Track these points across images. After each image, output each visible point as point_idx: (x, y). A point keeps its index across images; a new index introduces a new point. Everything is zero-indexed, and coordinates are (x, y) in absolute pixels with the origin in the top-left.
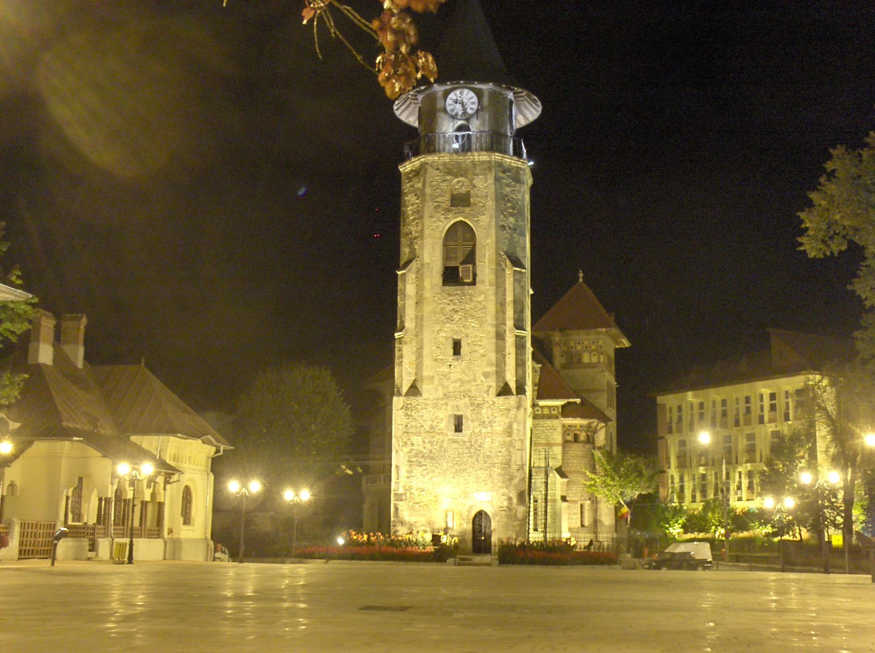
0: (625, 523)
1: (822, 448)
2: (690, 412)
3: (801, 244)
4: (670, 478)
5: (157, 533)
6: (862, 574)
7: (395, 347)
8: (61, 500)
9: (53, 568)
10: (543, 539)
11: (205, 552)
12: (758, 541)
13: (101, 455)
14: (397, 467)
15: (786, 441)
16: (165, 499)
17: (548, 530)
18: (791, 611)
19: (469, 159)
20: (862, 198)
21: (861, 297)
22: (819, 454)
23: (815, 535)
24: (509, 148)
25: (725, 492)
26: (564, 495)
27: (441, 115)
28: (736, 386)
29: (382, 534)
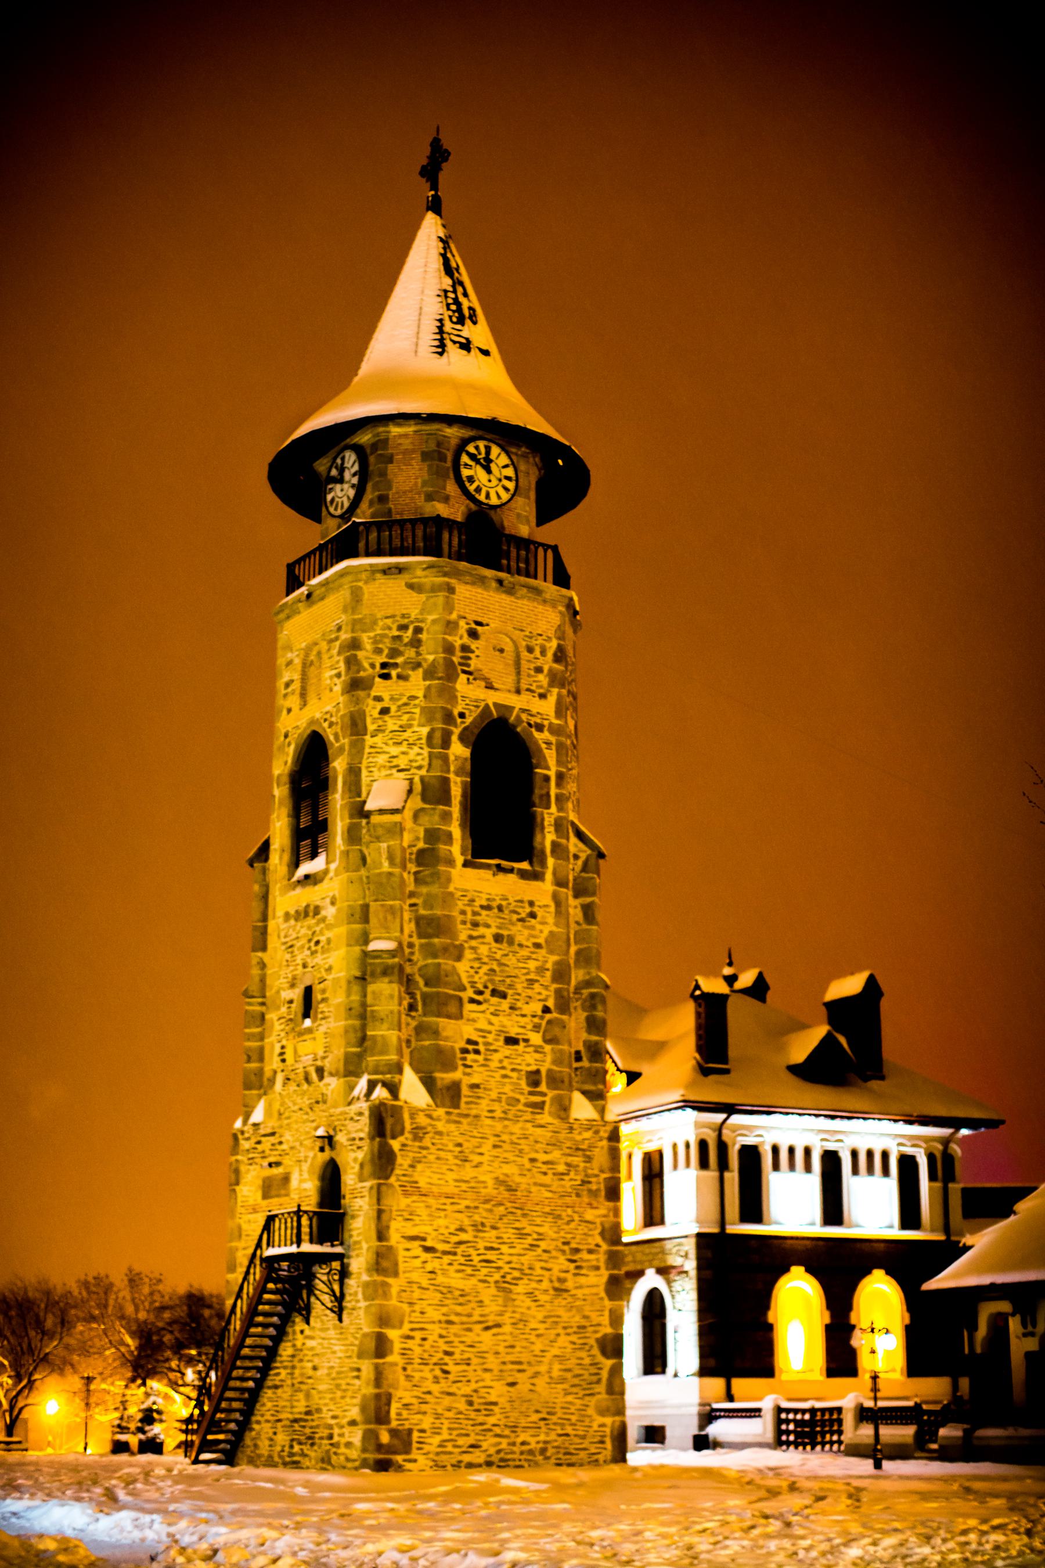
1: (356, 1338)
10: (871, 1440)
12: (560, 612)
14: (400, 569)
21: (605, 1336)
22: (691, 1265)
25: (635, 1538)
26: (669, 1433)
27: (492, 513)
28: (305, 519)
29: (803, 1420)
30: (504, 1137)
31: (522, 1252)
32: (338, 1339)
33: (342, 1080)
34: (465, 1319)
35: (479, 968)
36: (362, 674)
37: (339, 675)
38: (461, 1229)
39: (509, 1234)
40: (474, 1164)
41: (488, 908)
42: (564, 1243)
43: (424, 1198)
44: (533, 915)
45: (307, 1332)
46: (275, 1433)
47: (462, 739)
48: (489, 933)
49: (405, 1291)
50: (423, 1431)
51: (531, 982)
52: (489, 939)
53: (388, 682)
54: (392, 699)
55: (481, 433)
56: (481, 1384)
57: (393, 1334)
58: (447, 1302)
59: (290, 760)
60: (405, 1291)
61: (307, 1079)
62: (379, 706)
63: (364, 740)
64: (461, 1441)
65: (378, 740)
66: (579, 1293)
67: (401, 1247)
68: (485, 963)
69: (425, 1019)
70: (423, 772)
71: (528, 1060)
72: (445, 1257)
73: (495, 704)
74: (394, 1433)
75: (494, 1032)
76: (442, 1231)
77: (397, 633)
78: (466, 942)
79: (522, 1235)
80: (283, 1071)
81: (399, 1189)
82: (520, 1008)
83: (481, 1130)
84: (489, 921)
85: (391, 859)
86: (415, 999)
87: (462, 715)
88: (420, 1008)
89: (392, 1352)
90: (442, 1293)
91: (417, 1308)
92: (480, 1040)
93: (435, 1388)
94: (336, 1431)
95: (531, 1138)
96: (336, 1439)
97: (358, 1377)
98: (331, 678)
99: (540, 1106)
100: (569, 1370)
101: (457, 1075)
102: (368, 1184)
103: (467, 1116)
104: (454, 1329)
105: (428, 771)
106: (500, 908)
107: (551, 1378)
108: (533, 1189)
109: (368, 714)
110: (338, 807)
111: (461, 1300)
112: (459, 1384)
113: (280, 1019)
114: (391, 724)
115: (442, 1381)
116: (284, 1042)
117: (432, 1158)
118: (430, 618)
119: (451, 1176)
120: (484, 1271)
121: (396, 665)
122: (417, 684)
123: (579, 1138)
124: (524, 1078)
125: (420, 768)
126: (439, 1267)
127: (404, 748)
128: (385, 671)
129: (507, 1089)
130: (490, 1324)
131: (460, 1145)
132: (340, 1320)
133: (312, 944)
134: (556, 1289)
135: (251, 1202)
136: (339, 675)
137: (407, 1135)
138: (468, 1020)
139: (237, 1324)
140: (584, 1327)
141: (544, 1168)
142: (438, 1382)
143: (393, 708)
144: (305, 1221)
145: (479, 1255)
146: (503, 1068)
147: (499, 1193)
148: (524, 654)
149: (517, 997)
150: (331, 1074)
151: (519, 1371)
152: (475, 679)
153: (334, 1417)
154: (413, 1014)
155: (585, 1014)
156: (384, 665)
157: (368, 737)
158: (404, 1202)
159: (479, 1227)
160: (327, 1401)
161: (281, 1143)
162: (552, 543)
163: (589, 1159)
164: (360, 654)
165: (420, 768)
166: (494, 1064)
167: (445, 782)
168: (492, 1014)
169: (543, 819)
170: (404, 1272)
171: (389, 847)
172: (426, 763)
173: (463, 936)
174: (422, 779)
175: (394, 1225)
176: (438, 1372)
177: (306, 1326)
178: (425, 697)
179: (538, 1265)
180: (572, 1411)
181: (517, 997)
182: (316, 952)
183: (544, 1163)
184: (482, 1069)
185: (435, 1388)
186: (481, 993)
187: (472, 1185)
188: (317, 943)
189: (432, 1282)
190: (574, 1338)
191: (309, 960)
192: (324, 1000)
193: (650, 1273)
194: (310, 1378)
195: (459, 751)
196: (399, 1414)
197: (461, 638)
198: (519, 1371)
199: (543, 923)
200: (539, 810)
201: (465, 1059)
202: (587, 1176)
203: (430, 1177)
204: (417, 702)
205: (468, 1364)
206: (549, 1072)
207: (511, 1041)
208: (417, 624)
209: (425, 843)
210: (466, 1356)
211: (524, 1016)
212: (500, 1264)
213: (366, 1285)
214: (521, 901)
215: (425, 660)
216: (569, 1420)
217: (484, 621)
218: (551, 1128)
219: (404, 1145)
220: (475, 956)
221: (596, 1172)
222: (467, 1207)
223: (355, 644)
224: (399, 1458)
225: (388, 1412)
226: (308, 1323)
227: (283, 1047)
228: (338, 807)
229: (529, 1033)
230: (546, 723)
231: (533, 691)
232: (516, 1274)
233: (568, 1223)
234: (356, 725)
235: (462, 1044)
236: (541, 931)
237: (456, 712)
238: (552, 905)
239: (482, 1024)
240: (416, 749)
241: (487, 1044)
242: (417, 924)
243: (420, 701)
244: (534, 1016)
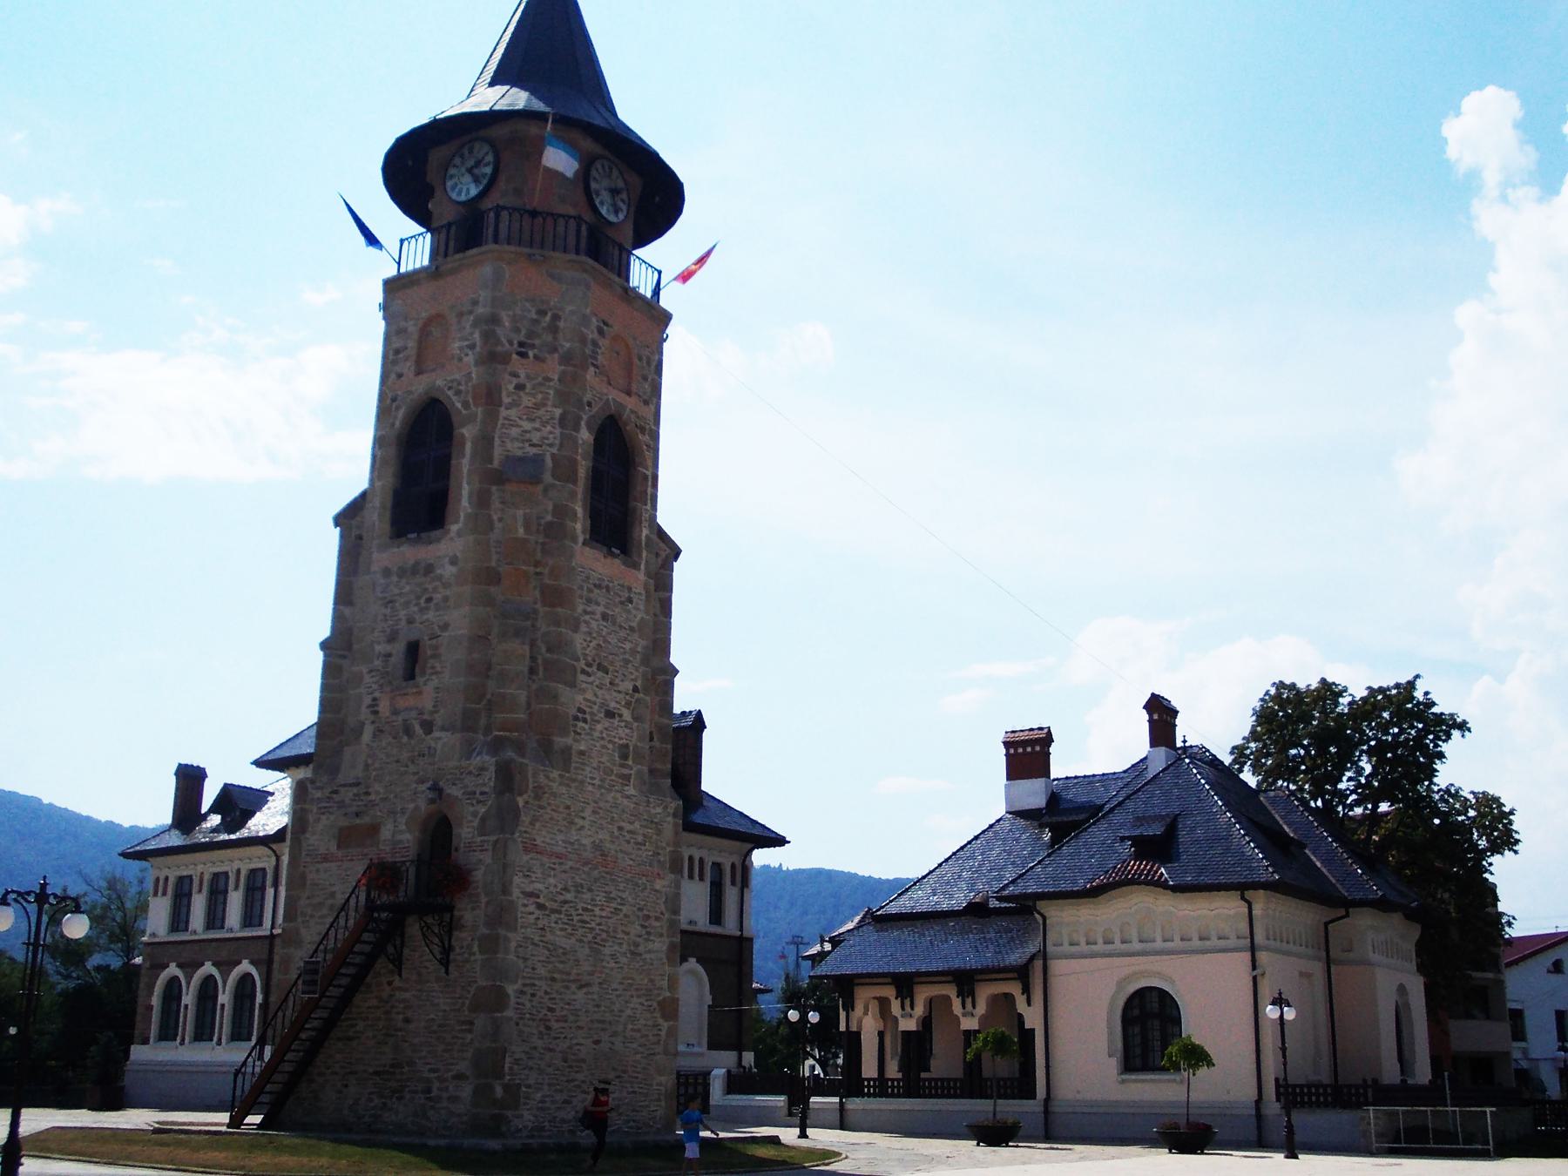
2: (1036, 732)
3: (1436, 764)
4: (219, 1007)
5: (550, 220)
6: (902, 1044)
7: (221, 1152)
8: (260, 1005)
9: (803, 1143)
11: (867, 987)
30: (602, 804)
31: (610, 915)
32: (442, 992)
33: (458, 735)
34: (564, 977)
35: (590, 642)
36: (499, 349)
37: (472, 347)
38: (566, 889)
39: (600, 898)
40: (578, 826)
41: (598, 586)
42: (639, 909)
43: (539, 856)
44: (630, 601)
46: (346, 1086)
47: (589, 428)
48: (600, 609)
49: (521, 946)
50: (529, 1086)
51: (627, 662)
52: (598, 616)
53: (524, 361)
54: (528, 377)
55: (607, 153)
56: (574, 1041)
58: (553, 959)
59: (398, 424)
60: (521, 946)
61: (408, 731)
62: (515, 381)
63: (498, 411)
64: (558, 1097)
65: (513, 413)
66: (648, 956)
67: (520, 902)
68: (594, 638)
69: (545, 683)
70: (554, 450)
71: (622, 734)
72: (553, 916)
73: (613, 399)
74: (506, 1088)
75: (598, 704)
76: (552, 889)
77: (535, 317)
78: (581, 615)
79: (610, 899)
80: (373, 722)
81: (521, 845)
82: (618, 685)
83: (584, 796)
84: (600, 600)
85: (527, 527)
87: (589, 404)
88: (541, 673)
90: (549, 950)
91: (529, 963)
92: (587, 710)
93: (539, 1043)
94: (436, 1085)
95: (620, 807)
96: (435, 1093)
97: (470, 1031)
98: (461, 348)
99: (627, 778)
100: (639, 1031)
101: (569, 741)
103: (574, 780)
104: (557, 986)
105: (558, 450)
106: (608, 588)
107: (625, 1037)
108: (620, 855)
109: (503, 387)
110: (465, 471)
111: (563, 959)
112: (558, 1041)
113: (371, 671)
114: (527, 401)
115: (545, 1037)
116: (377, 694)
117: (547, 817)
118: (570, 308)
119: (560, 837)
120: (581, 931)
121: (533, 346)
122: (554, 368)
123: (653, 811)
124: (617, 750)
125: (551, 445)
126: (547, 924)
127: (537, 425)
128: (523, 350)
129: (604, 759)
130: (583, 983)
131: (568, 807)
132: (447, 972)
133: (422, 601)
134: (633, 953)
135: (322, 850)
136: (472, 347)
137: (530, 793)
138: (580, 690)
140: (650, 990)
141: (628, 836)
142: (542, 1039)
143: (528, 386)
145: (578, 915)
146: (603, 738)
147: (595, 857)
148: (636, 360)
149: (616, 674)
150: (443, 729)
151: (603, 1030)
152: (600, 373)
153: (431, 1070)
154: (534, 677)
155: (658, 698)
156: (521, 344)
157: (502, 409)
159: (578, 888)
160: (424, 1054)
161: (368, 793)
162: (659, 269)
163: (659, 832)
164: (499, 331)
165: (551, 445)
166: (596, 734)
167: (573, 464)
168: (597, 686)
169: (641, 516)
170: (522, 927)
171: (525, 515)
172: (557, 442)
173: (580, 609)
174: (553, 455)
175: (517, 880)
176: (542, 1029)
177: (397, 978)
178: (559, 380)
179: (620, 928)
180: (638, 1070)
181: (616, 674)
182: (427, 609)
183: (628, 832)
184: (587, 737)
185: (539, 1043)
186: (589, 665)
187: (576, 847)
188: (429, 600)
189: (542, 939)
190: (642, 1000)
191: (417, 617)
192: (434, 656)
193: (173, 965)
194: (400, 1030)
195: (585, 436)
196: (511, 1069)
197: (592, 332)
198: (603, 1030)
199: (638, 609)
200: (639, 504)
201: (576, 726)
202: (657, 847)
203: (545, 837)
204: (551, 384)
205: (566, 1021)
206: (636, 746)
207: (610, 714)
208: (555, 311)
209: (553, 516)
210: (564, 1013)
211: (619, 692)
212: (593, 925)
214: (623, 586)
215: (562, 346)
216: (637, 1078)
217: (610, 322)
218: (634, 799)
219: (527, 802)
220: (587, 630)
221: (664, 845)
222: (571, 868)
223: (494, 320)
224: (509, 1113)
226: (400, 975)
227: (375, 699)
228: (465, 471)
229: (623, 709)
230: (647, 427)
231: (639, 396)
232: (604, 935)
233: (643, 891)
234: (491, 397)
235: (573, 711)
236: (635, 616)
237: (585, 400)
238: (643, 592)
239: (589, 696)
240: (549, 428)
241: (592, 714)
242: (542, 593)
243: (555, 383)
244: (627, 694)
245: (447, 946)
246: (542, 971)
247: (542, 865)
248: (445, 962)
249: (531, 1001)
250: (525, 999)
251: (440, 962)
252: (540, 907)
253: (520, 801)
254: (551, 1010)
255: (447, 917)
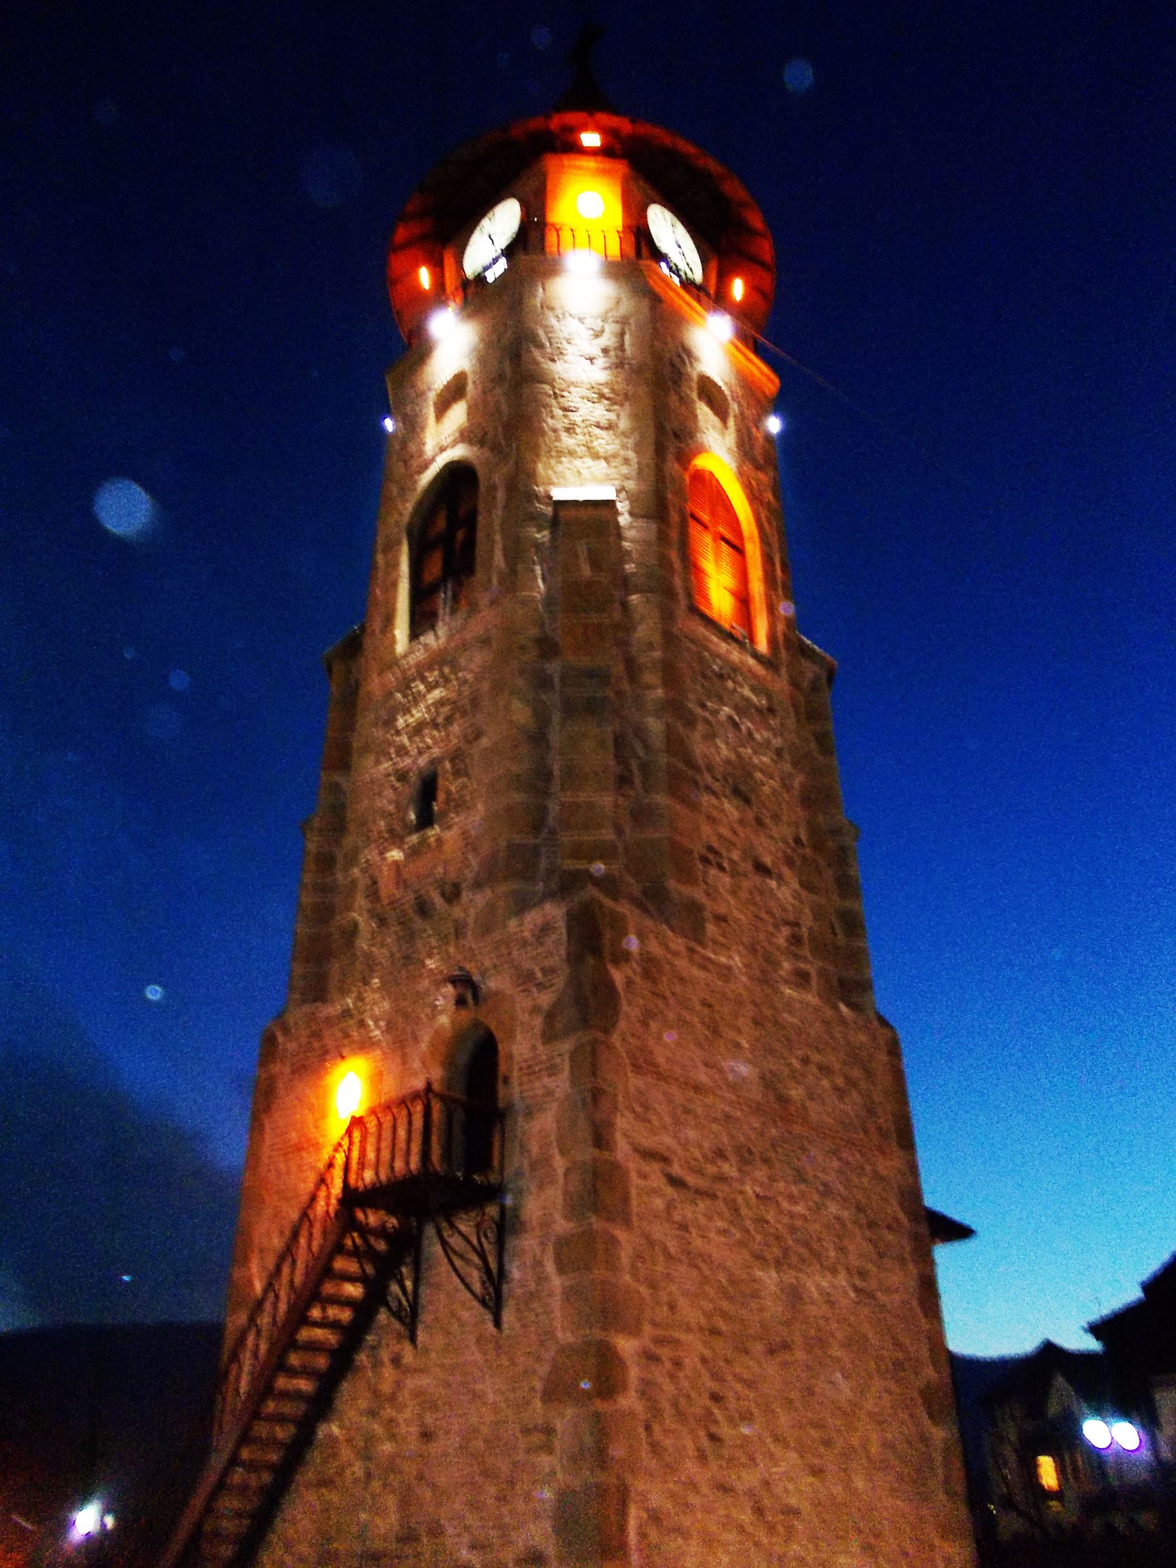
0: (700, 528)
12: (103, 1525)
13: (550, 314)
15: (733, 1064)
16: (495, 261)
17: (294, 1215)
18: (400, 899)
19: (799, 1159)
20: (749, 1124)
23: (343, 1299)
24: (781, 549)
28: (470, 243)
38: (720, 1154)
45: (408, 1356)
57: (626, 1346)
86: (357, 1174)
89: (625, 1388)
102: (566, 1046)
132: (497, 1323)
139: (257, 1346)
144: (437, 1107)
158: (635, 1082)
175: (623, 1122)
177: (407, 1347)
213: (563, 1245)
225: (622, 1529)
226: (413, 1339)
245: (493, 1265)
246: (691, 1314)
247: (670, 1100)
248: (493, 1301)
249: (672, 1377)
250: (659, 1375)
251: (483, 1303)
252: (675, 1182)
253: (618, 976)
254: (716, 1398)
255: (492, 1211)
